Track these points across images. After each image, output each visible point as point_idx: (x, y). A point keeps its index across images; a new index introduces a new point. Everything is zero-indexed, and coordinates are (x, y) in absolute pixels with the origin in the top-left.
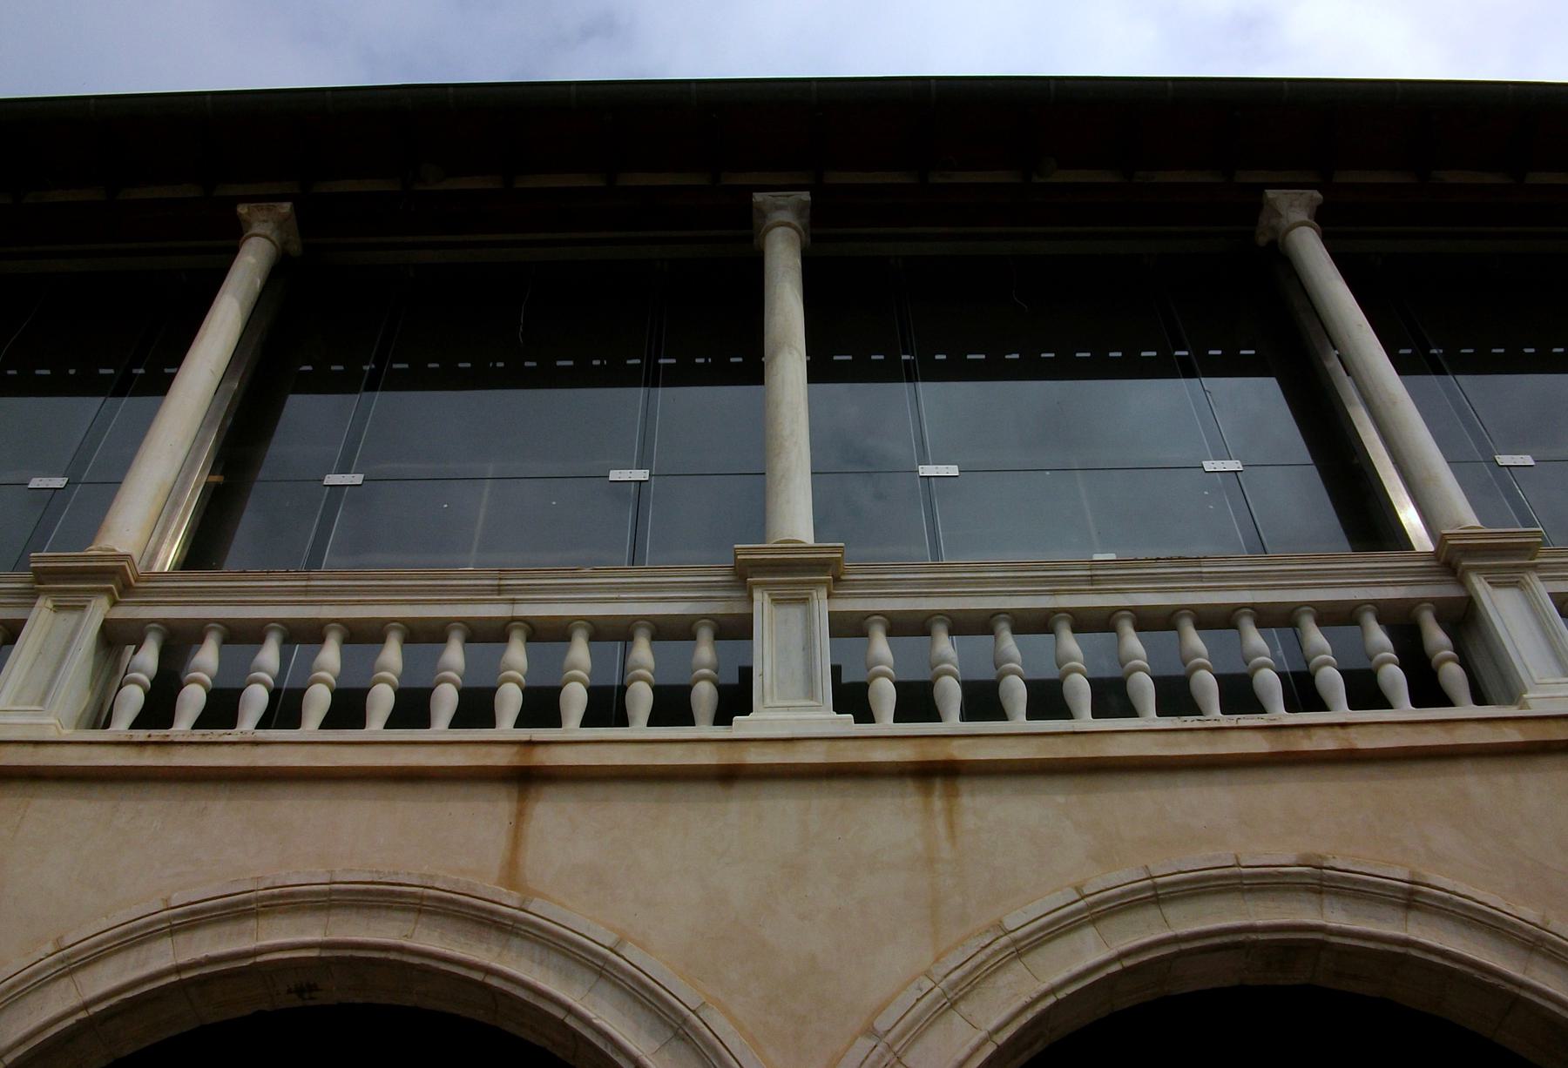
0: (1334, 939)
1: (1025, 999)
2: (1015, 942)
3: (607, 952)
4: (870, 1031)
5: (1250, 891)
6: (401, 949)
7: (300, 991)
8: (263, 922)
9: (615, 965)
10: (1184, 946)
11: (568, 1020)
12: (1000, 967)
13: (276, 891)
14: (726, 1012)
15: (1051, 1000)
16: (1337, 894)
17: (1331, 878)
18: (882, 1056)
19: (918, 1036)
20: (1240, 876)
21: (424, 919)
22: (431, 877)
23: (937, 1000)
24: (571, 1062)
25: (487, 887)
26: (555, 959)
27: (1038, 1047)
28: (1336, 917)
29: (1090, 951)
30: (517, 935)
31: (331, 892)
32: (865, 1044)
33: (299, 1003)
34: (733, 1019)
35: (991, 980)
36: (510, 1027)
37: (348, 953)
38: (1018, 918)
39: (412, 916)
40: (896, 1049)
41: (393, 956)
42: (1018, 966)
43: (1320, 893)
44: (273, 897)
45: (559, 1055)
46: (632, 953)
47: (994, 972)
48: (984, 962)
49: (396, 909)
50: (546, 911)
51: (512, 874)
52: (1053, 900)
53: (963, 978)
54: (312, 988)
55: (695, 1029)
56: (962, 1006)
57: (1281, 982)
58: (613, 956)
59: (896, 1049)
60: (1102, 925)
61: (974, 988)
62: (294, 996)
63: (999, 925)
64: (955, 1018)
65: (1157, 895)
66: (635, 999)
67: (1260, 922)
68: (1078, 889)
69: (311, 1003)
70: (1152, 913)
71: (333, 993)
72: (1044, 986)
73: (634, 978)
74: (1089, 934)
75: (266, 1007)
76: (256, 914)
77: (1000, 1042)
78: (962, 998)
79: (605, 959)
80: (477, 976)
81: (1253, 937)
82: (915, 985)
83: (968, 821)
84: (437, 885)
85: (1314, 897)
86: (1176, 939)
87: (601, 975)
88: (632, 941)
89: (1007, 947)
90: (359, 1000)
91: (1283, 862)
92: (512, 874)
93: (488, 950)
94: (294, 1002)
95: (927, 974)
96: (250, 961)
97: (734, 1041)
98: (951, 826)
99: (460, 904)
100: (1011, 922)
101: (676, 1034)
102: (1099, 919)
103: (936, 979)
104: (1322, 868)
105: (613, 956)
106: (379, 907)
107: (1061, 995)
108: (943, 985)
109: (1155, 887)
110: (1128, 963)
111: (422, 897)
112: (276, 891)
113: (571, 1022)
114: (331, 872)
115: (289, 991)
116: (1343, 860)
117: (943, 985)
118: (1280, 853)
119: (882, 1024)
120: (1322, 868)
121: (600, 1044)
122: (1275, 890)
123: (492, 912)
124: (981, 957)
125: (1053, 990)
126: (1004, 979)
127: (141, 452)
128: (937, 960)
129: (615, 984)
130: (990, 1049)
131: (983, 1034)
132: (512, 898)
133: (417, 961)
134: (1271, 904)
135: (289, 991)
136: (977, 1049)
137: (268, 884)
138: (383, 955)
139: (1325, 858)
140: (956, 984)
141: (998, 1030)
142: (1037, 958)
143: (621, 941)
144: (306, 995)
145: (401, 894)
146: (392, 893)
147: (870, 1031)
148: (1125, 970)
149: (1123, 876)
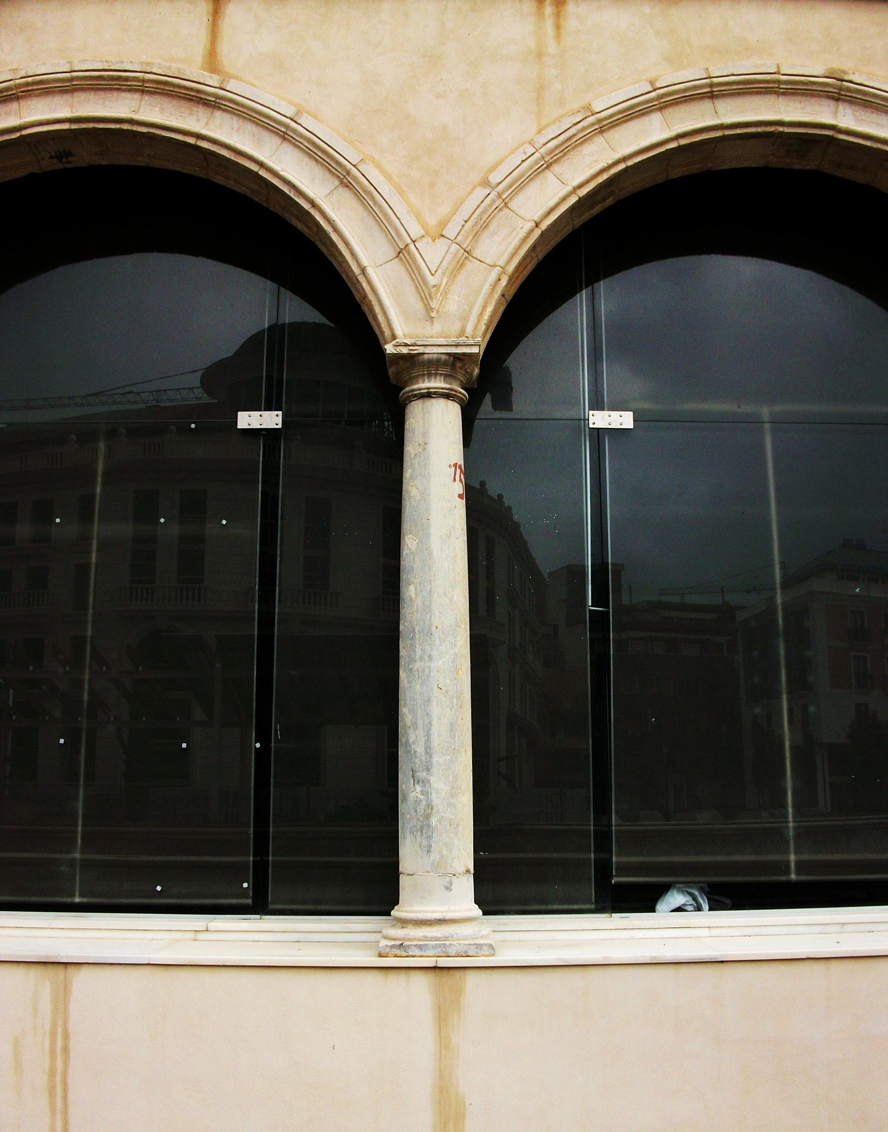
0: (842, 137)
1: (604, 164)
2: (600, 121)
3: (288, 121)
4: (485, 183)
5: (784, 94)
6: (131, 121)
7: (59, 157)
8: (23, 103)
9: (295, 131)
10: (727, 132)
11: (260, 173)
12: (585, 140)
13: (30, 79)
14: (378, 166)
15: (622, 166)
16: (850, 102)
17: (848, 89)
18: (494, 201)
19: (520, 188)
20: (779, 82)
21: (147, 98)
22: (148, 64)
23: (537, 162)
24: (265, 205)
25: (193, 71)
26: (250, 127)
27: (610, 202)
28: (847, 119)
29: (655, 132)
30: (219, 108)
31: (72, 79)
32: (482, 192)
33: (59, 166)
34: (388, 177)
35: (579, 149)
36: (219, 180)
37: (91, 125)
38: (605, 102)
39: (137, 96)
40: (504, 196)
41: (126, 127)
42: (600, 140)
43: (838, 100)
44: (27, 84)
45: (256, 199)
46: (306, 121)
47: (582, 143)
48: (574, 135)
49: (124, 90)
50: (243, 88)
51: (212, 62)
52: (631, 89)
53: (557, 147)
54: (69, 154)
55: (355, 179)
56: (556, 168)
57: (796, 167)
58: (293, 124)
59: (504, 196)
60: (667, 112)
61: (565, 155)
62: (55, 161)
63: (588, 107)
64: (549, 176)
65: (713, 92)
66: (310, 156)
67: (787, 118)
68: (652, 83)
69: (68, 166)
70: (707, 105)
71: (84, 157)
72: (618, 156)
73: (309, 140)
74: (656, 117)
75: (35, 170)
76: (16, 98)
77: (581, 195)
78: (556, 161)
79: (287, 127)
80: (191, 140)
81: (781, 129)
82: (521, 150)
83: (571, 23)
84: (154, 71)
85: (832, 103)
86: (722, 127)
87: (284, 139)
88: (307, 112)
89: (593, 125)
90: (105, 163)
91: (813, 74)
92: (212, 62)
93: (198, 120)
94: (57, 166)
95: (531, 143)
96: (18, 135)
97: (384, 188)
98: (558, 27)
99: (174, 85)
100: (597, 106)
101: (342, 182)
102: (665, 107)
103: (538, 146)
104: (842, 80)
105: (293, 124)
106: (111, 89)
107: (630, 163)
108: (542, 150)
109: (711, 85)
110: (683, 142)
111: (144, 81)
112: (30, 79)
113: (263, 173)
114: (70, 63)
115: (51, 157)
116: (861, 76)
117: (542, 150)
118: (813, 67)
119: (494, 178)
120: (842, 80)
121: (285, 189)
122: (803, 95)
123: (198, 91)
124: (573, 131)
125: (624, 159)
126: (588, 149)
127: (403, 505)
128: (539, 132)
129: (295, 145)
130: (573, 200)
131: (569, 188)
132: (213, 80)
133: (144, 130)
134: (799, 106)
135: (51, 157)
136: (564, 199)
137: (23, 74)
138: (118, 126)
139: (845, 73)
140: (552, 151)
141: (580, 186)
142: (614, 135)
143: (298, 113)
144: (64, 160)
145: (127, 79)
146: (119, 78)
147: (485, 183)
148: (680, 148)
149: (688, 74)
